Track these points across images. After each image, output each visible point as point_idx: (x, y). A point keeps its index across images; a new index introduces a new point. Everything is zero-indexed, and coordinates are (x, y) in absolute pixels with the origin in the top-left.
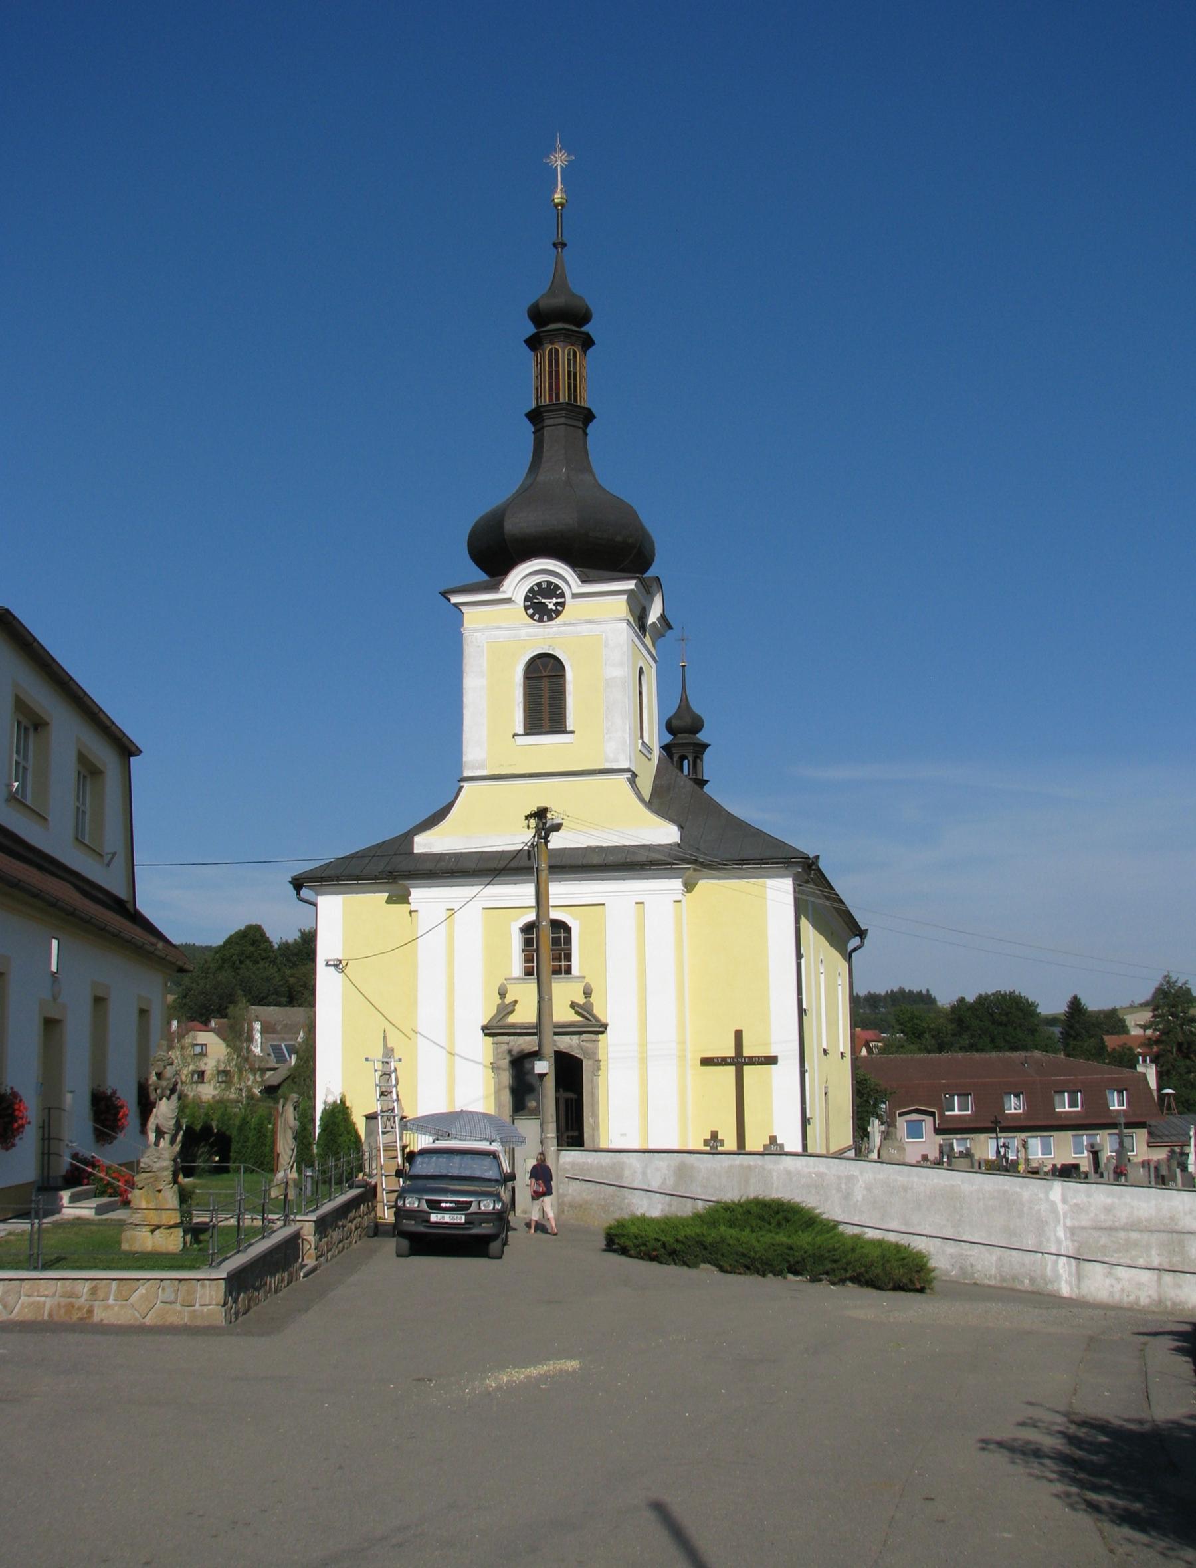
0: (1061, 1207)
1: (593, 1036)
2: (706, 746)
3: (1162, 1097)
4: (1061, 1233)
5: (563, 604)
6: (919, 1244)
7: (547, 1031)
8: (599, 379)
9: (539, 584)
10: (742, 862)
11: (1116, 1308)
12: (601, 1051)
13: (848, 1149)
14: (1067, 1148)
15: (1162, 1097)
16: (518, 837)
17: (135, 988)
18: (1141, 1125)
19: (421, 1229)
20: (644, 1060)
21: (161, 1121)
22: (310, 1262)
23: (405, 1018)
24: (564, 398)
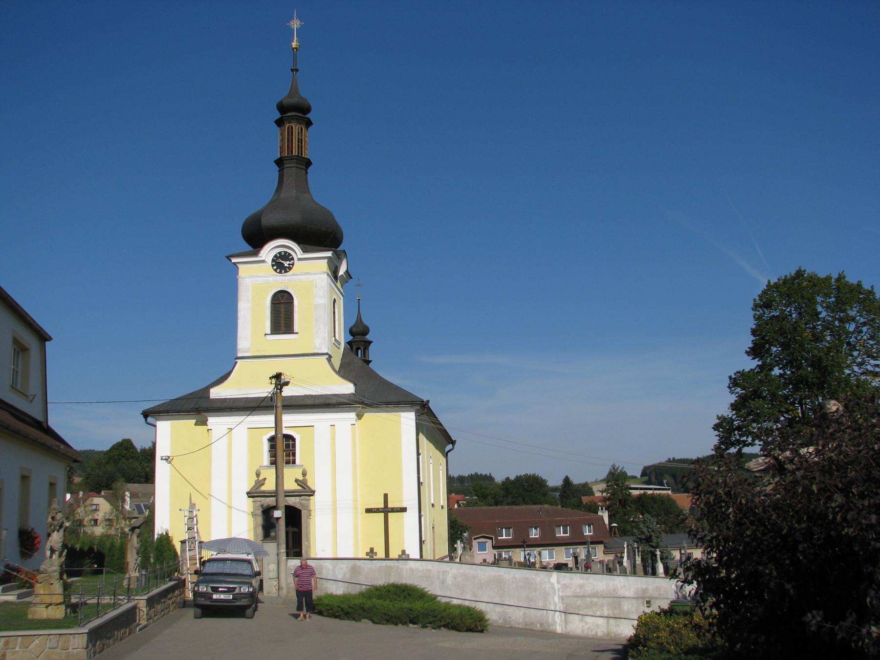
0: (557, 586)
1: (307, 497)
2: (370, 342)
3: (611, 528)
4: (556, 599)
5: (293, 264)
6: (481, 607)
7: (281, 495)
8: (314, 142)
9: (280, 253)
10: (388, 403)
11: (586, 638)
13: (446, 557)
14: (561, 555)
15: (611, 528)
16: (265, 389)
17: (57, 471)
18: (600, 543)
19: (208, 603)
20: (335, 510)
21: (53, 544)
22: (144, 623)
23: (204, 488)
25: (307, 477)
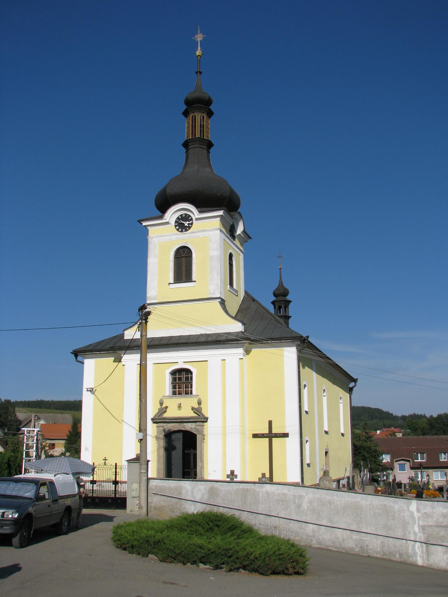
0: (416, 514)
2: (290, 302)
4: (416, 529)
5: (192, 224)
9: (181, 215)
12: (205, 430)
20: (224, 434)
24: (198, 135)
25: (201, 406)
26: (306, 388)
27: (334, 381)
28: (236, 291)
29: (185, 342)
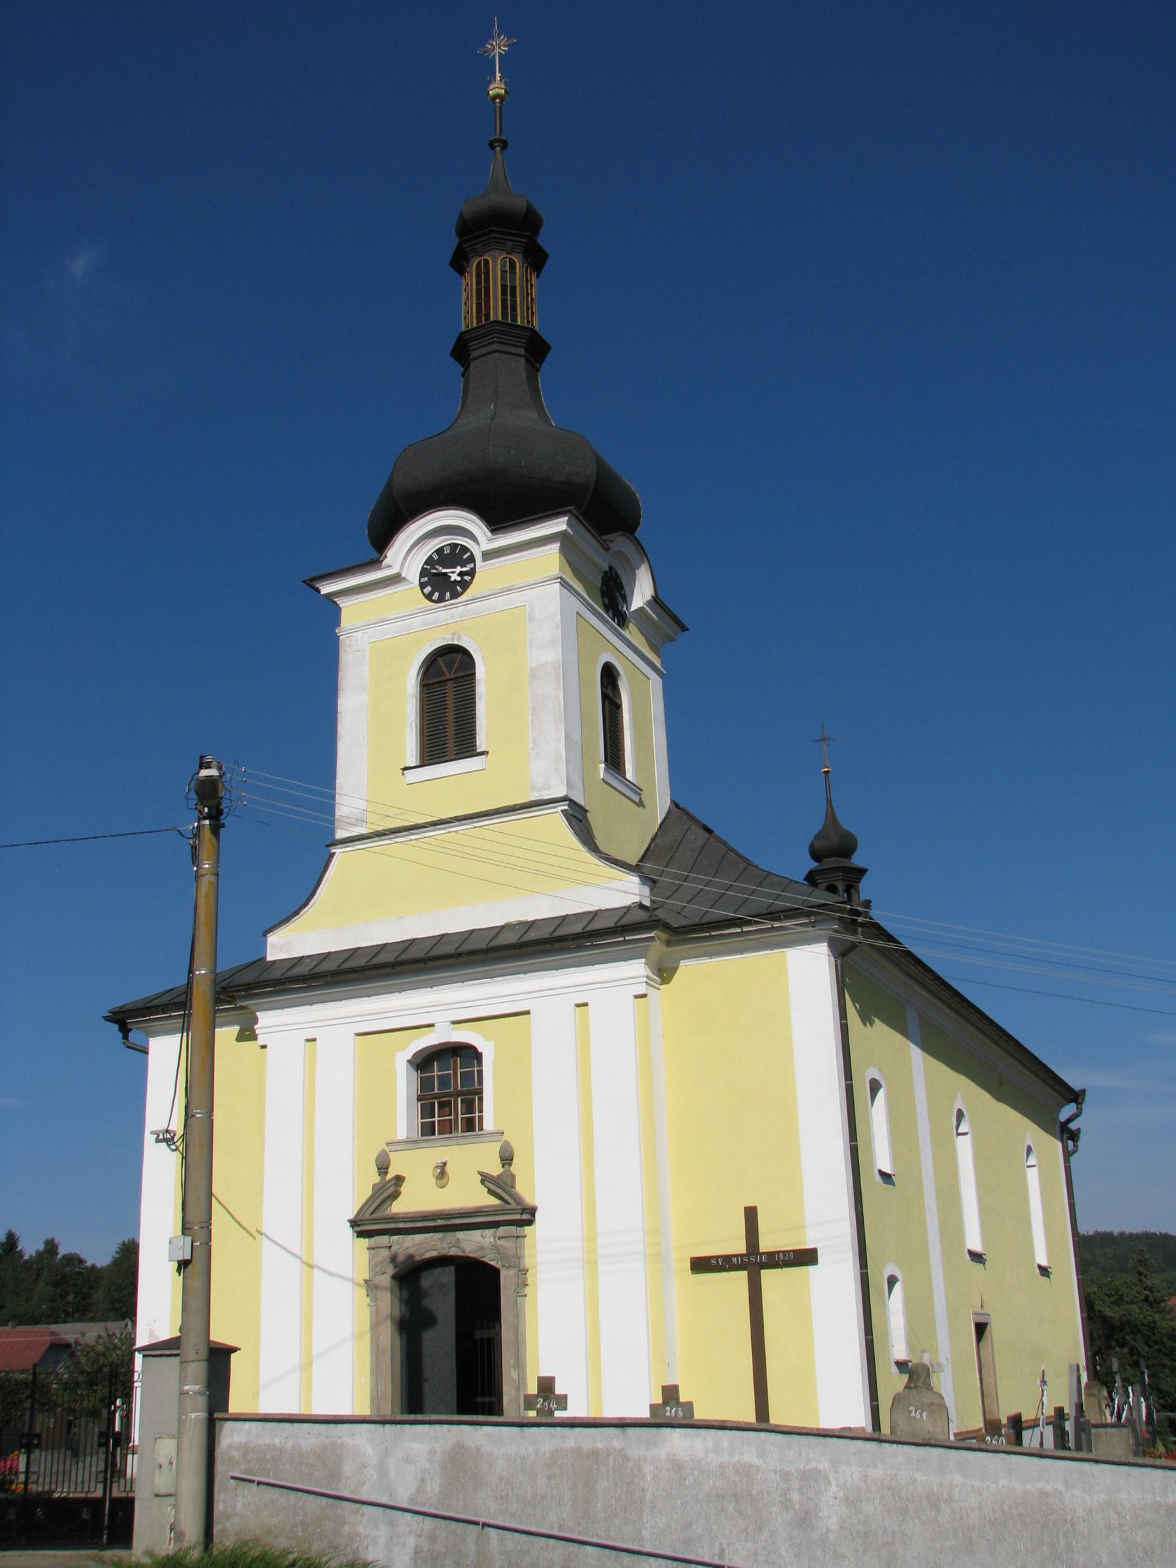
2: (862, 872)
5: (472, 573)
9: (440, 551)
12: (527, 1252)
20: (591, 1263)
24: (496, 314)
25: (514, 1168)
26: (881, 1094)
27: (1001, 1090)
28: (637, 790)
29: (453, 951)
